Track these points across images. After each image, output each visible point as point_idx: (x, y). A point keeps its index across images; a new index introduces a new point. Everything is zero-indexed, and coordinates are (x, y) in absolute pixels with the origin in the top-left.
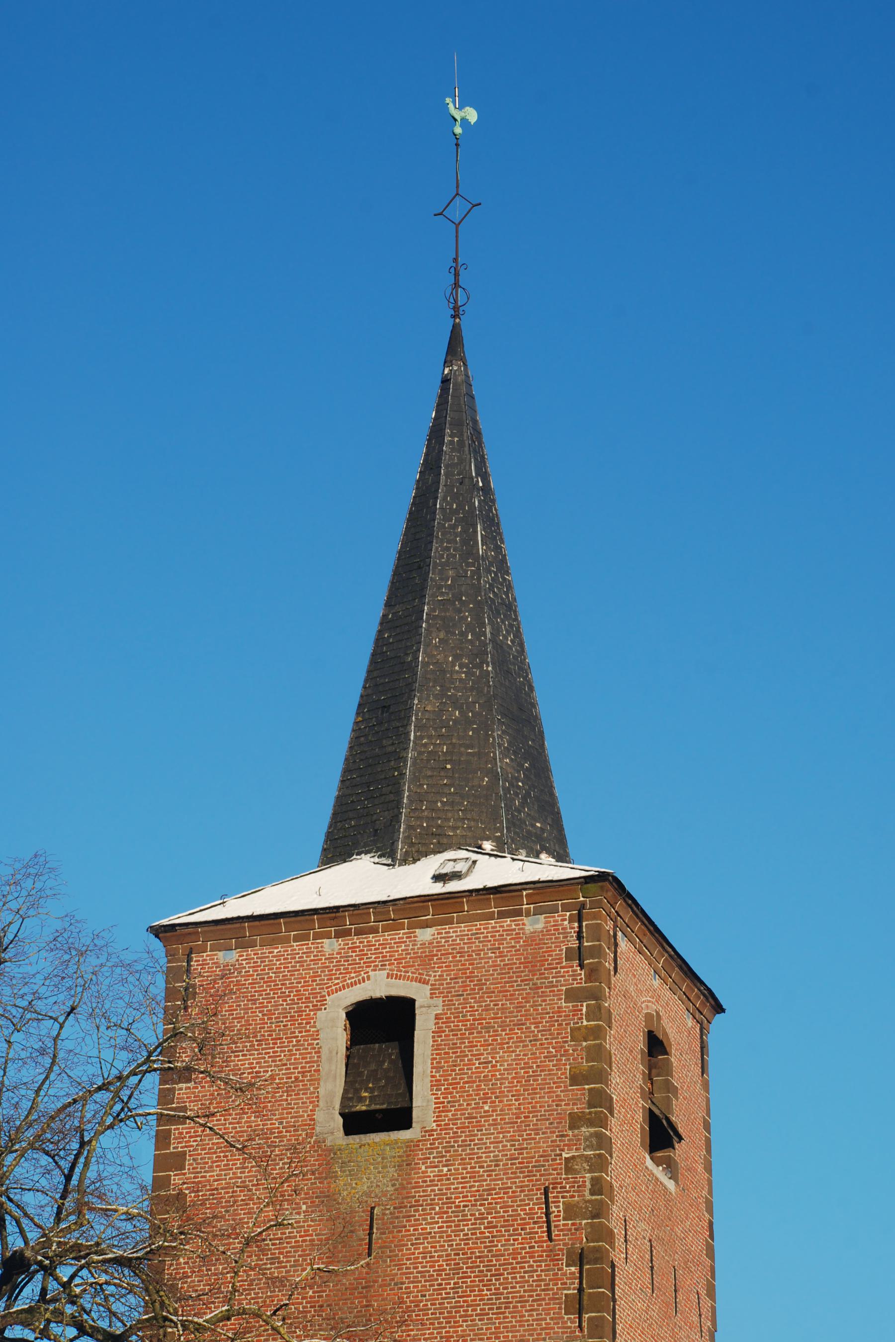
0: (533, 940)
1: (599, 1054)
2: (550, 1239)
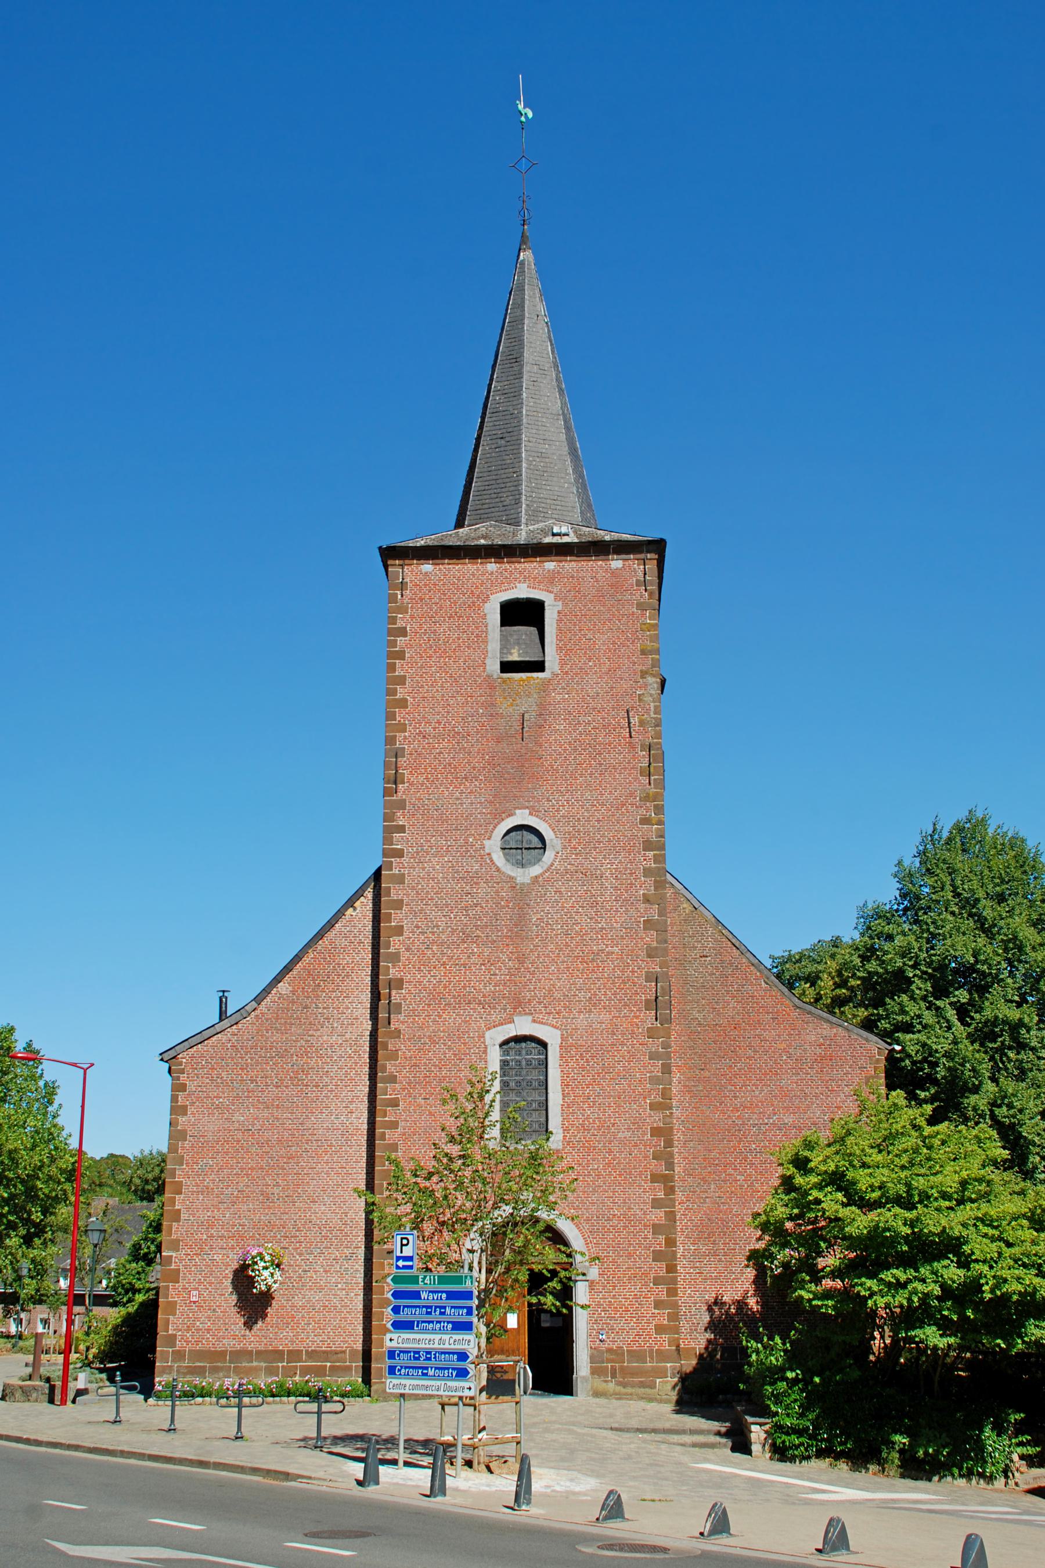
0: (614, 573)
1: (666, 1094)
2: (631, 737)
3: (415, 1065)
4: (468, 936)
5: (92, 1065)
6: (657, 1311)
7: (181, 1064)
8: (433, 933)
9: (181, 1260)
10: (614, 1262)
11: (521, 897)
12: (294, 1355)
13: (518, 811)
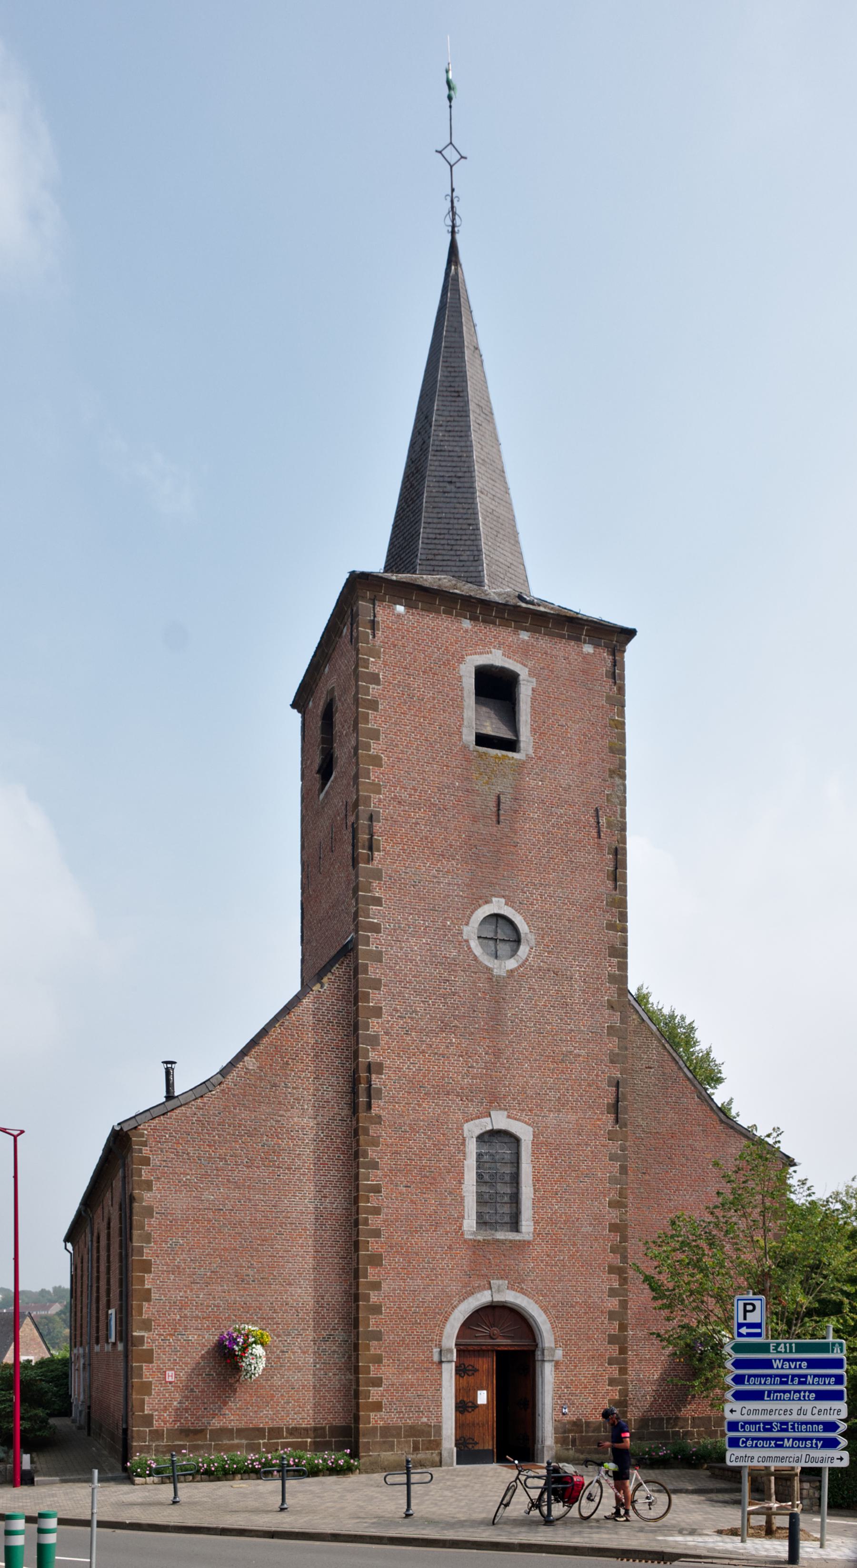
0: (585, 657)
3: (396, 1153)
4: (446, 1025)
5: (22, 1132)
6: (610, 1388)
7: (142, 1135)
8: (412, 1019)
9: (154, 1341)
10: (576, 1344)
11: (497, 988)
12: (276, 1432)
13: (494, 899)
